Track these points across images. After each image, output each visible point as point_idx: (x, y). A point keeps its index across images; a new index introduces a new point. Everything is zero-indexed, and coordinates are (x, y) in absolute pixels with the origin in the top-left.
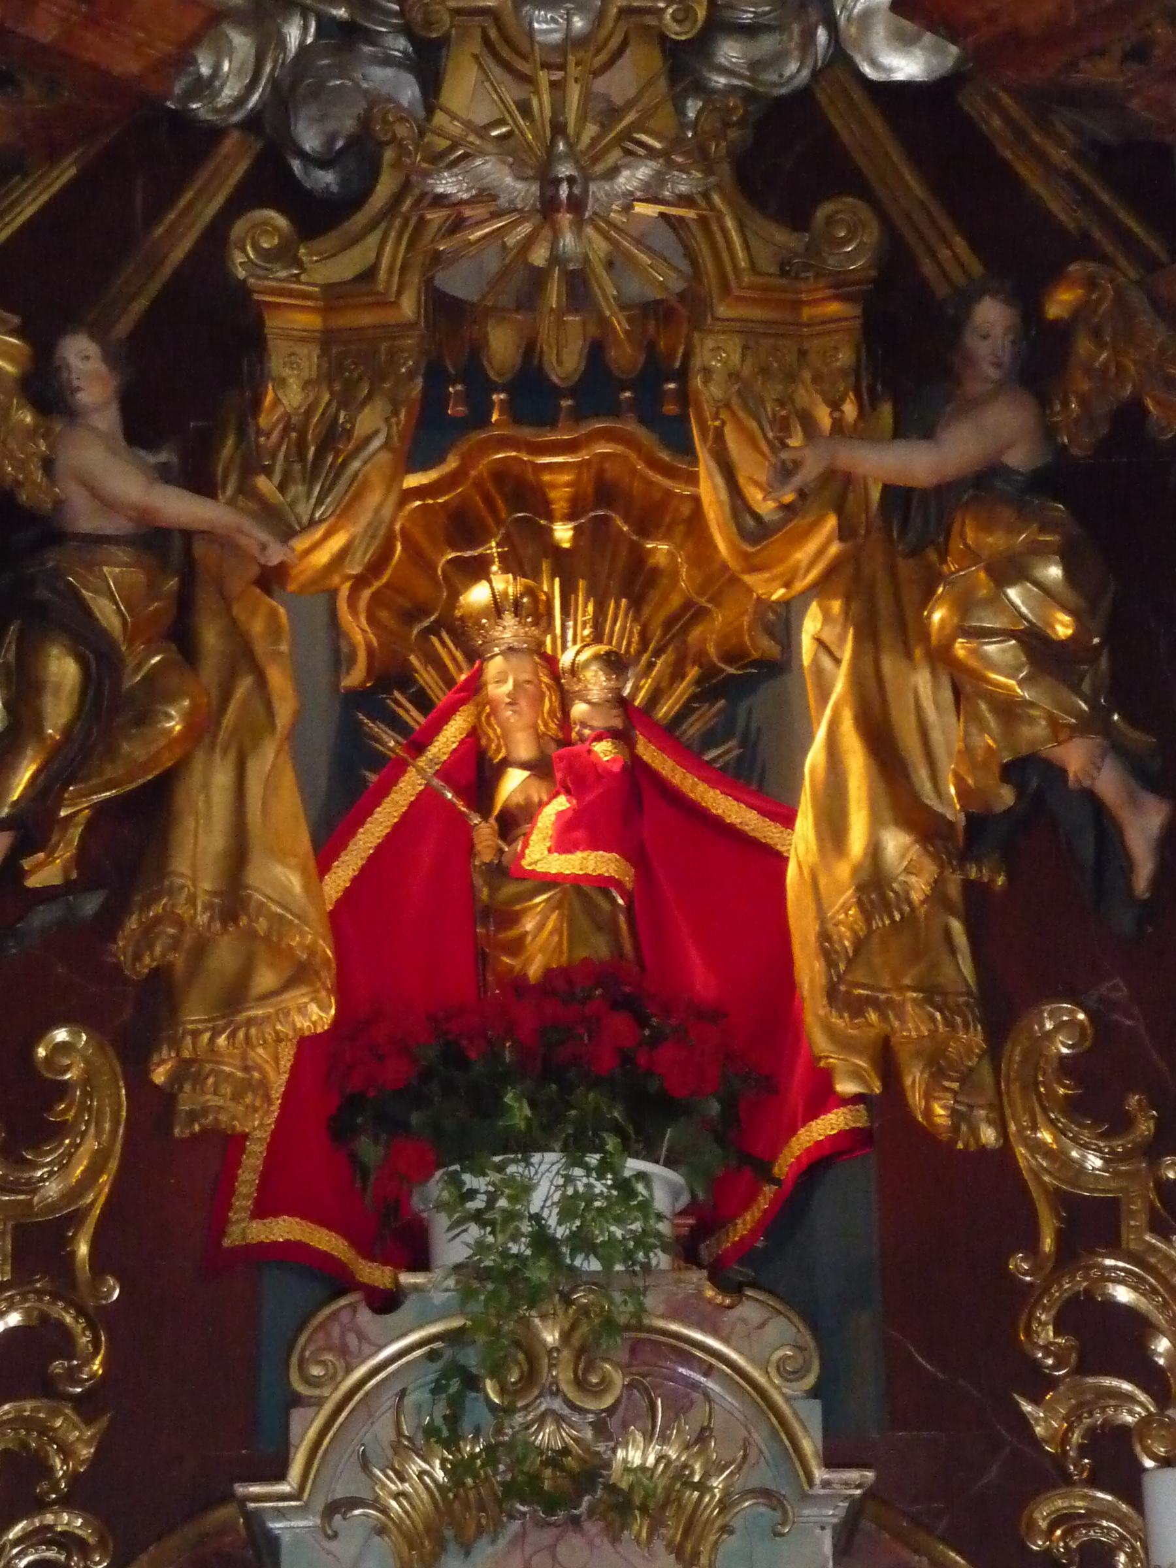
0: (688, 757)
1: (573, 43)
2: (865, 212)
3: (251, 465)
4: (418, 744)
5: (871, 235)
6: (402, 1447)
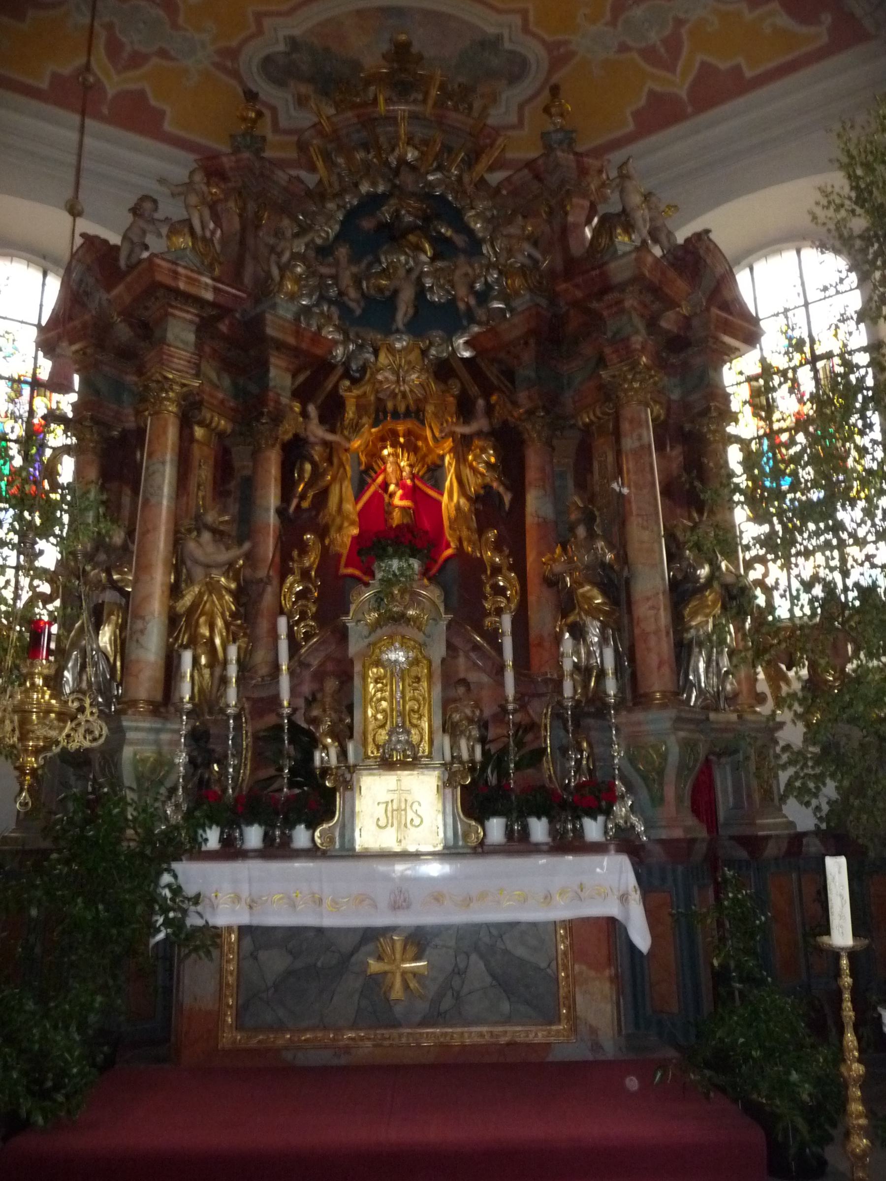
0: (425, 484)
1: (404, 348)
2: (457, 381)
3: (343, 428)
4: (374, 480)
5: (459, 385)
6: (370, 611)
